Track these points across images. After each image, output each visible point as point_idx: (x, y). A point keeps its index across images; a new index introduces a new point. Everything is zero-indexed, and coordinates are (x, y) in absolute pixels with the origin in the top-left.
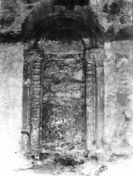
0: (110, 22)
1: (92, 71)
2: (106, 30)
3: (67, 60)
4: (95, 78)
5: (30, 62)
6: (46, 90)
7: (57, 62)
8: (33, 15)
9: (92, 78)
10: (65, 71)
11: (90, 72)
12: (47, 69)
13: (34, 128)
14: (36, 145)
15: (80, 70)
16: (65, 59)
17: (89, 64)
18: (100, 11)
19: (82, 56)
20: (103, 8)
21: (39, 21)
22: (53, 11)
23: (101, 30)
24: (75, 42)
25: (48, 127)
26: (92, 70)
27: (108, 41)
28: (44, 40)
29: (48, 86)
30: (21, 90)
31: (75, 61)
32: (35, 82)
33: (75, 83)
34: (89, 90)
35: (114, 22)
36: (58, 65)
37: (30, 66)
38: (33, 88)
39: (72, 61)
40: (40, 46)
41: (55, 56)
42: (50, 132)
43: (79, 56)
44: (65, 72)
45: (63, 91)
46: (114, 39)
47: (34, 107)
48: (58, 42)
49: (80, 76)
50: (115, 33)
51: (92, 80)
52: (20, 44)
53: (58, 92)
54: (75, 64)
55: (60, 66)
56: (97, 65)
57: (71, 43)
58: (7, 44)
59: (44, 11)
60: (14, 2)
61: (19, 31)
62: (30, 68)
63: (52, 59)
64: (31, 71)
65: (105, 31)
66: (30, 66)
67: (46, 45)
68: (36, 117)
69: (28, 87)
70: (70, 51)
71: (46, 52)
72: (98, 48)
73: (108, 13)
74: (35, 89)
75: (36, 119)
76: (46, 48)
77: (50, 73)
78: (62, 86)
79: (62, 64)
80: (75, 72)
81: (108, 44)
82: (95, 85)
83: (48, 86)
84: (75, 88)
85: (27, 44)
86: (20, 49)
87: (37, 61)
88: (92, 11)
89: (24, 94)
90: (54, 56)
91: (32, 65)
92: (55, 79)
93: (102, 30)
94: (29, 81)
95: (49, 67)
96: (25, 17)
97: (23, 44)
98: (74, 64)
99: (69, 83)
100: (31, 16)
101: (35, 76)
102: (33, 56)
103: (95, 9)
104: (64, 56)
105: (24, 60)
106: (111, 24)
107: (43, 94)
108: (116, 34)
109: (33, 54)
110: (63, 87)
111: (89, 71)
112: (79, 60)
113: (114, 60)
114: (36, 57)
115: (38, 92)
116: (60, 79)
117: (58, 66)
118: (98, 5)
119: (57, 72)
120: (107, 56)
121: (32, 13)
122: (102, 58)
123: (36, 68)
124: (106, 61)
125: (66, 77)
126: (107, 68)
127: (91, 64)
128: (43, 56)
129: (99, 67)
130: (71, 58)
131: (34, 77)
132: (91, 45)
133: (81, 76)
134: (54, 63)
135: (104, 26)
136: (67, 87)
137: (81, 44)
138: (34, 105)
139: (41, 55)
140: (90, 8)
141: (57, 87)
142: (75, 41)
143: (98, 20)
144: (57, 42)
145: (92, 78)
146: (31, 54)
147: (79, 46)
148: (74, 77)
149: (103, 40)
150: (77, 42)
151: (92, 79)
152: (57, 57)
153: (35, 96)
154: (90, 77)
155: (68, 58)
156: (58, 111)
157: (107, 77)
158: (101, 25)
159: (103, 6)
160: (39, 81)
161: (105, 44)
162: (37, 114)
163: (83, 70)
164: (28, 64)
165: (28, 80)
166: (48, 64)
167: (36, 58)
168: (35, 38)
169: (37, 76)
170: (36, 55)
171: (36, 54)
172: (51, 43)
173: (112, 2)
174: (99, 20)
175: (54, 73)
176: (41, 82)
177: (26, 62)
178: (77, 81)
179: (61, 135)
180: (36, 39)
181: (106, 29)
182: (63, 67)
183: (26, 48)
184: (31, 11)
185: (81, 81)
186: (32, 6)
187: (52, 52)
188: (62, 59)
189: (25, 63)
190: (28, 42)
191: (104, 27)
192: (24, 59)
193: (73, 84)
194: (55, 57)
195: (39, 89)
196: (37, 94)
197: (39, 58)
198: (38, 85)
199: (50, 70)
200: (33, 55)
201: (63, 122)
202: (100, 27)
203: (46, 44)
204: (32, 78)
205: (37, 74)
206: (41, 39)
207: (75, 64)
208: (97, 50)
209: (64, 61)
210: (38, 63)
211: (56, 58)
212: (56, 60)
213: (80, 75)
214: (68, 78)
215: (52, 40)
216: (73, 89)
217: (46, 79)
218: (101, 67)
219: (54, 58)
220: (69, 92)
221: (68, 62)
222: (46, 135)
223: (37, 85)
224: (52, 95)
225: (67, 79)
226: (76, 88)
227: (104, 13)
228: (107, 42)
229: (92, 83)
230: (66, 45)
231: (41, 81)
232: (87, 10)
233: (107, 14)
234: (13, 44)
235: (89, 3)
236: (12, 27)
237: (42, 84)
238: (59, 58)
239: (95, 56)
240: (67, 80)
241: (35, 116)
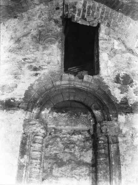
0: (123, 93)
1: (105, 150)
2: (120, 101)
3: (73, 136)
4: (108, 158)
5: (30, 135)
6: (46, 174)
7: (62, 139)
8: (38, 82)
9: (105, 159)
10: (71, 150)
11: (103, 151)
12: (50, 146)
15: (89, 150)
16: (71, 136)
17: (101, 140)
18: (112, 82)
19: (92, 132)
20: (114, 78)
21: (45, 89)
22: (61, 80)
23: (114, 101)
24: (84, 116)
26: (104, 148)
27: (122, 113)
28: (49, 110)
29: (49, 168)
30: (16, 169)
31: (83, 138)
32: (34, 161)
33: (83, 166)
34: (101, 173)
35: (128, 93)
36: (63, 143)
37: (29, 139)
38: (31, 169)
39: (79, 138)
40: (44, 117)
41: (61, 131)
43: (88, 132)
44: (71, 152)
45: (68, 176)
46: (129, 111)
48: (65, 114)
49: (89, 158)
50: (129, 105)
51: (105, 161)
52: (20, 112)
53: (62, 177)
54: (84, 142)
55: (65, 144)
56: (111, 140)
57: (79, 116)
58: (6, 112)
59: (51, 79)
60: (19, 69)
61: (22, 98)
62: (29, 142)
63: (57, 135)
64: (30, 146)
65: (118, 103)
66: (29, 139)
67: (50, 118)
69: (24, 166)
70: (77, 125)
71: (50, 125)
72: (110, 120)
73: (120, 84)
74: (33, 170)
76: (50, 120)
77: (53, 152)
78: (68, 169)
79: (68, 141)
80: (84, 152)
81: (122, 116)
82: (108, 167)
83: (49, 168)
84: (83, 172)
85: (29, 113)
86: (19, 118)
87: (39, 133)
88: (103, 81)
89: (19, 174)
90: (59, 131)
91: (32, 138)
92: (58, 161)
93: (114, 101)
94: (26, 158)
95: (52, 144)
96: (30, 84)
97: (24, 113)
98: (82, 141)
99: (76, 166)
100: (36, 83)
101: (34, 152)
102: (34, 126)
103: (106, 79)
104: (70, 132)
105: (23, 131)
106: (122, 96)
107: (42, 179)
108: (131, 106)
109: (35, 124)
110: (68, 170)
111: (101, 149)
112: (88, 137)
113: (130, 135)
114: (38, 129)
115: (36, 174)
116: (65, 160)
118: (109, 76)
119: (62, 151)
120: (122, 130)
121: (38, 80)
122: (116, 133)
123: (36, 142)
124: (121, 137)
125: (72, 158)
127: (102, 140)
128: (46, 128)
129: (113, 143)
130: (78, 134)
131: (34, 154)
132: (103, 117)
133: (91, 157)
134: (58, 139)
135: (116, 97)
136: (74, 171)
137: (91, 118)
139: (44, 127)
140: (101, 78)
141: (61, 171)
142: (84, 114)
143: (109, 90)
144: (64, 115)
145: (105, 159)
146: (33, 124)
147: (88, 119)
148: (82, 158)
149: (116, 112)
150: (86, 116)
151: (104, 160)
152: (63, 132)
153: (32, 178)
154: (102, 157)
155: (75, 135)
157: (123, 156)
158: (113, 96)
159: (114, 77)
160: (39, 160)
161: (119, 116)
163: (93, 150)
164: (27, 136)
165: (26, 157)
166: (50, 141)
167: (38, 130)
168: (39, 107)
169: (37, 153)
170: (39, 126)
171: (38, 125)
172: (57, 116)
173: (124, 73)
174: (111, 90)
175: (58, 152)
176: (41, 162)
177: (25, 134)
178: (86, 164)
180: (39, 108)
181: (119, 100)
182: (69, 145)
183: (27, 118)
184: (37, 78)
185: (90, 164)
186: (40, 74)
187: (56, 126)
188: (68, 136)
189: (24, 135)
190: (30, 111)
191: (116, 98)
192: (24, 129)
193: (81, 167)
194: (60, 133)
195: (38, 170)
196: (35, 176)
197: (41, 130)
198: (38, 165)
199: (52, 148)
200: (34, 126)
202: (113, 97)
203: (50, 116)
204: (31, 155)
205: (38, 150)
206: (46, 109)
207: (84, 142)
208: (109, 123)
209: (70, 137)
210: (39, 136)
211: (61, 134)
212: (61, 136)
213: (90, 157)
214: (75, 159)
215: (57, 112)
216: (81, 174)
217: (47, 159)
218: (115, 145)
219: (58, 134)
220: (76, 178)
221: (74, 139)
223: (36, 165)
225: (74, 161)
226: (84, 173)
227: (115, 84)
228: (121, 114)
229: (104, 165)
230: (74, 118)
231: (41, 160)
232: (97, 80)
233: (119, 85)
234: (12, 112)
235: (100, 73)
236: (14, 94)
237: (42, 165)
238: (64, 134)
239: (108, 130)
240: (73, 162)
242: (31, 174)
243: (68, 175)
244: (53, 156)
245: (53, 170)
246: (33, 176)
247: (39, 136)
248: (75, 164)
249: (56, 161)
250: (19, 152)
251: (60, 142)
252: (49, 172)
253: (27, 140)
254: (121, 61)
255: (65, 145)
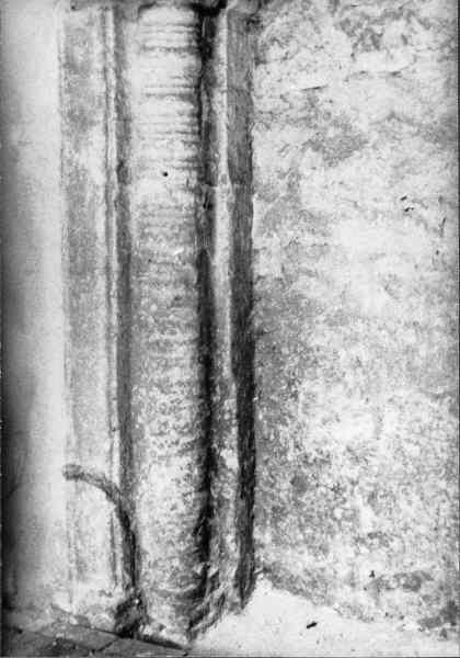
6: (270, 206)
13: (153, 452)
14: (171, 558)
25: (284, 452)
29: (282, 175)
42: (299, 484)
47: (151, 320)
68: (163, 387)
75: (164, 399)
83: (282, 175)
116: (362, 126)
117: (343, 25)
123: (152, 49)
126: (418, 70)
138: (147, 308)
156: (342, 353)
162: (167, 367)
179: (367, 515)
201: (378, 431)
222: (276, 503)
224: (308, 239)
225: (410, 122)
241: (158, 376)
242: (145, 221)
243: (379, 206)
244: (300, 104)
245: (301, 182)
246: (155, 231)
247: (108, 263)
248: (418, 141)
249: (309, 134)
250: (59, 118)
251: (331, 20)
252: (283, 194)
253: (92, 45)
254: (170, 137)
255: (358, 32)
